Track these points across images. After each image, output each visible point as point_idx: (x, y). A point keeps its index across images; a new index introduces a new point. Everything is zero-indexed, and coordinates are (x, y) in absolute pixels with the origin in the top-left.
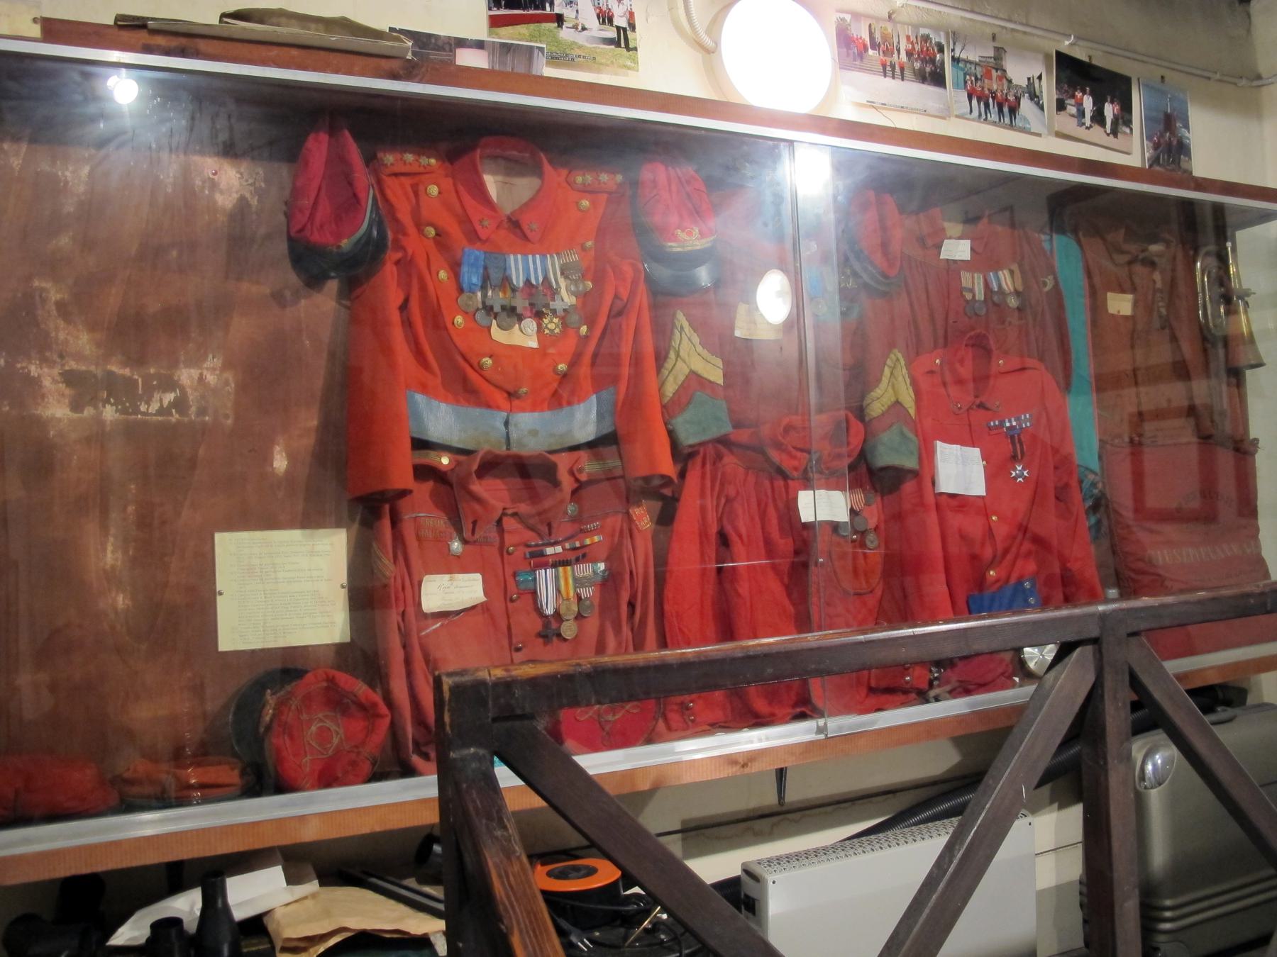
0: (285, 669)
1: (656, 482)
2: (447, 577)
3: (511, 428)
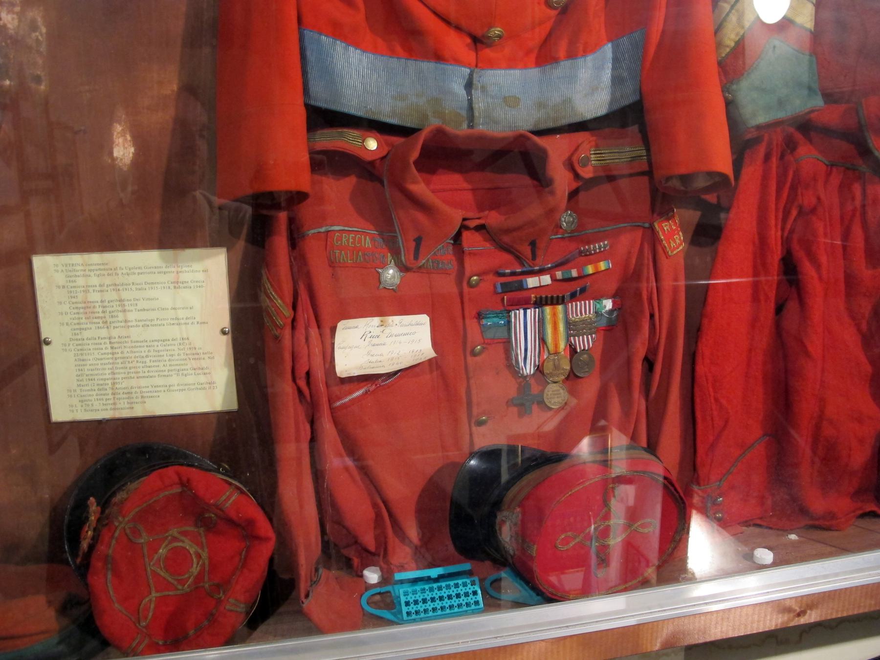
0: (133, 450)
1: (701, 183)
2: (376, 320)
3: (476, 94)
